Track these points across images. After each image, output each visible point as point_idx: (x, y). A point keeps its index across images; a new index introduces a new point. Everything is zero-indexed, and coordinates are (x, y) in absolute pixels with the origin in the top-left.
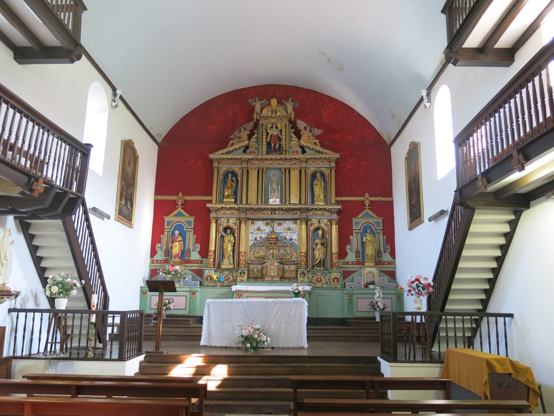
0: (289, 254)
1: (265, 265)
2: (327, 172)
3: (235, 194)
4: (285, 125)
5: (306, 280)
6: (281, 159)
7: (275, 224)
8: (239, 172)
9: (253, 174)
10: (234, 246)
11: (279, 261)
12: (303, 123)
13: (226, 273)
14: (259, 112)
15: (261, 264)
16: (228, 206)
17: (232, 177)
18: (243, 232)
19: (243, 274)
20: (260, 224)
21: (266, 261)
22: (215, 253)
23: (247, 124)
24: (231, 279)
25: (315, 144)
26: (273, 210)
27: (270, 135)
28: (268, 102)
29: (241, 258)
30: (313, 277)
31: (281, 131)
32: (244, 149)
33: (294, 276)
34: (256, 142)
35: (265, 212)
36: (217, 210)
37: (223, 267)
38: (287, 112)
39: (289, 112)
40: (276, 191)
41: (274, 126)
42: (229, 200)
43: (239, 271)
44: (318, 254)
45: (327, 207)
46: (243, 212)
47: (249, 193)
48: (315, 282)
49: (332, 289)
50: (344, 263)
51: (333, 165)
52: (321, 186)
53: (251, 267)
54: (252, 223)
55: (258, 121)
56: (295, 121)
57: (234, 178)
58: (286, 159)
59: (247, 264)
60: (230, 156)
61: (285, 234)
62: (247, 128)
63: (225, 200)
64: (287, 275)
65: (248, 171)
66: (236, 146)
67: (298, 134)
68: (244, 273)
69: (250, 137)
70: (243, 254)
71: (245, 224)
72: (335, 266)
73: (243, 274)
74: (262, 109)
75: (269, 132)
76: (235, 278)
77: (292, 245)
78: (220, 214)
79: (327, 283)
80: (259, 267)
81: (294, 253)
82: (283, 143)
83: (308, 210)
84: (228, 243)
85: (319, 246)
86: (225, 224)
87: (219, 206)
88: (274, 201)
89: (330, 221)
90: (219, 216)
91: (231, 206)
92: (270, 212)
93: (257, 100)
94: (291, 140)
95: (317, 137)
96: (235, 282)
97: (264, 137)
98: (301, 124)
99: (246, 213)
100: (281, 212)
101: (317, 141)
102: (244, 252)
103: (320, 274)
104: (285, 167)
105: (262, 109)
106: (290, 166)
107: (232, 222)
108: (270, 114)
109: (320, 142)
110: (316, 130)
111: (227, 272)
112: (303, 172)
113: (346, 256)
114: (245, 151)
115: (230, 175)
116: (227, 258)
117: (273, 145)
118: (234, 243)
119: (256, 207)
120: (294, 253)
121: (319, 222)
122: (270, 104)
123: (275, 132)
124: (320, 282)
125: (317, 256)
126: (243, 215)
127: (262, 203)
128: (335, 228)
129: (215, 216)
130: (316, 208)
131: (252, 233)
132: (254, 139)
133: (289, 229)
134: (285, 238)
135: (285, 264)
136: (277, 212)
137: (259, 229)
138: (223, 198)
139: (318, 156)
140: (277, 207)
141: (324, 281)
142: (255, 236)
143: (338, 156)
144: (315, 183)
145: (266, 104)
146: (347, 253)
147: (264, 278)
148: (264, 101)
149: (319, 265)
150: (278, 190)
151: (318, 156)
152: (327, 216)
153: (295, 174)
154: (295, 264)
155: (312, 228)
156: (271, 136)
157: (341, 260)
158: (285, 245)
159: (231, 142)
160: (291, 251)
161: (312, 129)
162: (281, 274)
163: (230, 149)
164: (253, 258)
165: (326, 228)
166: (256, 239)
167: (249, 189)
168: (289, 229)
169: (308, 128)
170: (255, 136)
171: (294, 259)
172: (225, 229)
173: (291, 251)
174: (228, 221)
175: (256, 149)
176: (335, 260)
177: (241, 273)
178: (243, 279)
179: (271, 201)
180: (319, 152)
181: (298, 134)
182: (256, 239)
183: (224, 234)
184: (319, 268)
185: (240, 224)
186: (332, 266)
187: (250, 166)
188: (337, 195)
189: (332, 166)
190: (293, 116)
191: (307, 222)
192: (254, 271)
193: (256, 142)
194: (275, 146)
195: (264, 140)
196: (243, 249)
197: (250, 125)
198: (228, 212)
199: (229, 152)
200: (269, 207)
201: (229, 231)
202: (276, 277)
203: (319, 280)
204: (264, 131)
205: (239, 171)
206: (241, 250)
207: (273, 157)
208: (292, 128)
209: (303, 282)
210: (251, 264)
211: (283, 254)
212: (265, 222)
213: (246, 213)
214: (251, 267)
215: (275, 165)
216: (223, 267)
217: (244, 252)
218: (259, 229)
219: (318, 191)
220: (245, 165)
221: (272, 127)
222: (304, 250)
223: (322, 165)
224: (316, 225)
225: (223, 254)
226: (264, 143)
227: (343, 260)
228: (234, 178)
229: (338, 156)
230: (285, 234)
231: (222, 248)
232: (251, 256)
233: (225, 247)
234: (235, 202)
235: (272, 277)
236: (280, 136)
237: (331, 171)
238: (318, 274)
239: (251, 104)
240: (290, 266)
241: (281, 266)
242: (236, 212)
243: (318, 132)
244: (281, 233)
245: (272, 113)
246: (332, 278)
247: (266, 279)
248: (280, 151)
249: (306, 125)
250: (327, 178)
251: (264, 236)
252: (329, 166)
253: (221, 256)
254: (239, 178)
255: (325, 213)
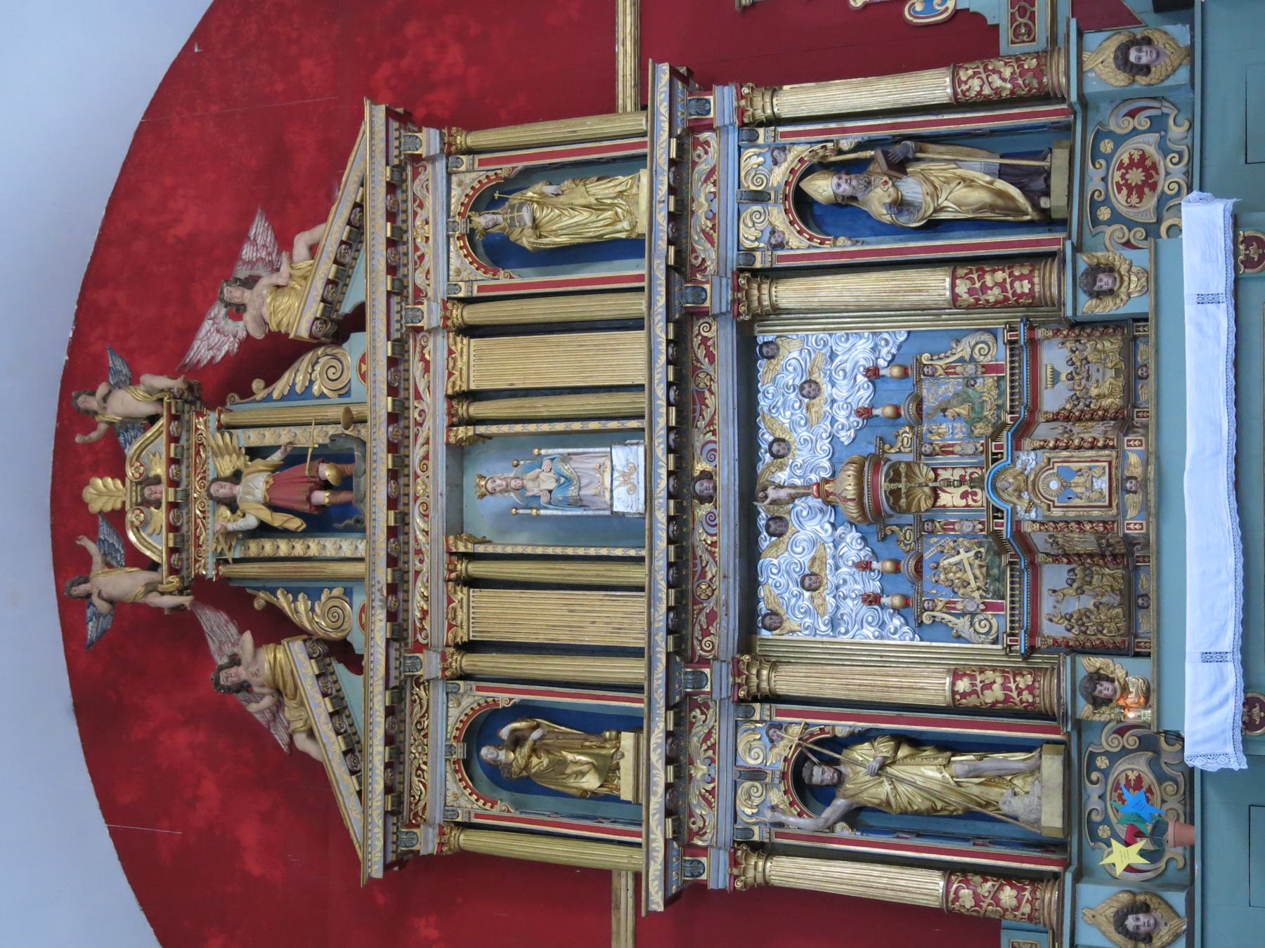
0: (970, 382)
1: (1040, 541)
2: (471, 176)
3: (592, 725)
4: (222, 428)
5: (1141, 258)
6: (393, 447)
7: (782, 477)
8: (472, 698)
9: (495, 613)
10: (916, 742)
11: (1005, 438)
12: (207, 325)
13: (1093, 802)
14: (146, 576)
15: (1034, 568)
16: (660, 775)
17: (499, 744)
18: (828, 685)
19: (1105, 689)
20: (779, 569)
21: (1006, 531)
22: (964, 871)
23: (213, 647)
24: (1137, 766)
25: (313, 249)
26: (684, 489)
27: (266, 515)
28: (104, 531)
29: (995, 694)
30: (1116, 218)
31: (254, 453)
32: (340, 669)
33: (1111, 345)
34: (314, 595)
35: (701, 536)
36: (683, 837)
37: (1052, 818)
38: (153, 419)
39: (149, 409)
40: (566, 469)
41: (223, 490)
42: (627, 765)
43: (1084, 709)
44: (961, 192)
45: (664, 148)
46: (699, 680)
47: (587, 640)
48: (1151, 201)
49: (1199, 81)
50: (1024, 31)
51: (429, 140)
52: (542, 202)
53: (1052, 630)
54: (775, 620)
55: (201, 589)
56: (194, 371)
57: (504, 733)
58: (393, 418)
59: (1037, 659)
60: (378, 753)
61: (841, 416)
62: (228, 650)
63: (626, 794)
64: (1105, 387)
65: (470, 647)
66: (320, 708)
67: (271, 355)
68: (1097, 677)
69: (275, 627)
70: (963, 685)
71: (774, 666)
72: (1039, 72)
73: (1105, 689)
74: (136, 559)
75: (251, 522)
76: (1131, 740)
77: (913, 371)
78: (711, 823)
79: (1158, 124)
80: (1054, 576)
81: (963, 350)
82: (311, 438)
83: (681, 268)
84: (893, 780)
85: (911, 188)
86: (776, 797)
87: (658, 829)
88: (622, 479)
89: (749, 127)
90: (726, 834)
91: (657, 759)
92: (702, 511)
93: (82, 589)
94: (307, 393)
95: (284, 243)
96: (1159, 741)
97: (283, 547)
98: (215, 340)
99: (705, 662)
100: (699, 439)
101: (301, 242)
102: (956, 675)
103: (1095, 175)
104: (443, 420)
105: (136, 559)
106: (442, 387)
107: (765, 750)
108: (160, 516)
109: (304, 227)
110: (248, 252)
111: (1093, 791)
112: (475, 314)
113: (978, 18)
114: (355, 663)
115: (487, 752)
116: (993, 793)
117: (322, 497)
118: (900, 739)
119: (664, 597)
120: (963, 350)
121: (759, 197)
122: (117, 518)
123: (257, 485)
124: (1150, 170)
125: (978, 196)
126: (717, 681)
127: (639, 560)
128: (796, 99)
129: (724, 857)
130: (672, 217)
131: (833, 623)
132: (298, 609)
133: (809, 389)
134: (865, 413)
135: (1034, 407)
136: (699, 467)
137: (811, 582)
138: (617, 799)
139: (378, 230)
140: (664, 462)
141: (1148, 144)
142: (851, 606)
143: (375, 116)
144: (527, 240)
145: (113, 540)
146: (956, 13)
147: (1130, 542)
148: (92, 547)
149: (1033, 182)
150: (566, 459)
151: (378, 230)
152: (723, 152)
153: (491, 364)
154: (1033, 343)
155: (798, 243)
156: (274, 508)
157: (1004, 46)
158: (908, 410)
159: (302, 742)
160: (949, 371)
161: (242, 272)
162: (1097, 431)
163: (330, 749)
164: (998, 622)
165: (799, 151)
166: (872, 600)
167: (565, 638)
168: (809, 389)
169: (233, 293)
170: (283, 601)
171: (1000, 354)
172: (807, 793)
173: (949, 371)
174: (756, 774)
175: (348, 593)
176: (1001, 78)
177: (1098, 703)
178: (1135, 684)
179: (627, 501)
180: (357, 229)
181: (271, 355)
182: (872, 600)
183: (840, 803)
184: (1058, 183)
185: (772, 698)
186: (1046, 96)
187: (436, 631)
188: (608, 106)
189: (435, 148)
190: (162, 382)
191: (755, 273)
192: (1085, 613)
193: (314, 595)
194: (325, 485)
195: (299, 548)
196: (933, 686)
197: (214, 622)
198: (700, 770)
199: (354, 749)
200: (661, 516)
201: (820, 775)
202: (1122, 456)
203: (1136, 176)
204: (253, 548)
205: (466, 702)
206: (942, 699)
207: (379, 491)
208: (247, 393)
209: (1154, 280)
210: (1034, 631)
211: (971, 423)
212: (765, 541)
213: (705, 662)
214: (1052, 630)
215: (431, 482)
216: (1052, 818)
217: (956, 675)
218: (811, 582)
219: (567, 214)
220: (430, 665)
221: (232, 504)
222: (936, 285)
223: (433, 206)
224: (778, 216)
225: (970, 815)
226: (313, 547)
227: (1005, 35)
228: (504, 733)
229: (375, 116)
230: (841, 416)
231: (928, 822)
232: (982, 635)
233: (920, 803)
234: (634, 723)
235: (1118, 485)
236: (276, 457)
237: (470, 151)
238: (1095, 183)
239: (106, 623)
240: (1045, 374)
241: (1043, 430)
242: (701, 722)
243: (260, 230)
244: (833, 438)
245: (158, 504)
246: (1118, 80)
247: (1133, 525)
248: (350, 459)
249: (219, 310)
250: (505, 170)
251: (852, 547)
252: (441, 165)
253: (983, 828)
254: (504, 699)
255: (703, 167)
